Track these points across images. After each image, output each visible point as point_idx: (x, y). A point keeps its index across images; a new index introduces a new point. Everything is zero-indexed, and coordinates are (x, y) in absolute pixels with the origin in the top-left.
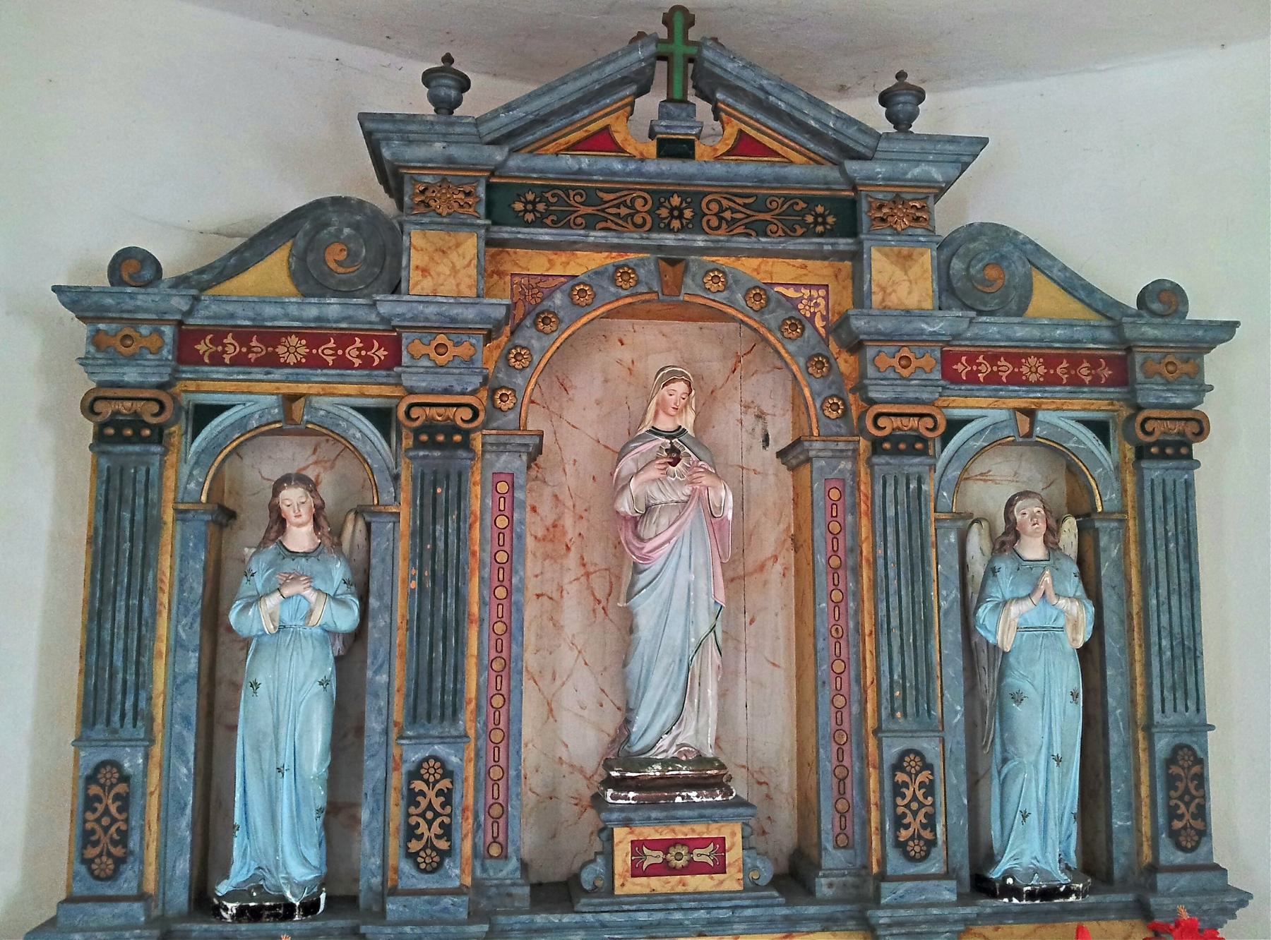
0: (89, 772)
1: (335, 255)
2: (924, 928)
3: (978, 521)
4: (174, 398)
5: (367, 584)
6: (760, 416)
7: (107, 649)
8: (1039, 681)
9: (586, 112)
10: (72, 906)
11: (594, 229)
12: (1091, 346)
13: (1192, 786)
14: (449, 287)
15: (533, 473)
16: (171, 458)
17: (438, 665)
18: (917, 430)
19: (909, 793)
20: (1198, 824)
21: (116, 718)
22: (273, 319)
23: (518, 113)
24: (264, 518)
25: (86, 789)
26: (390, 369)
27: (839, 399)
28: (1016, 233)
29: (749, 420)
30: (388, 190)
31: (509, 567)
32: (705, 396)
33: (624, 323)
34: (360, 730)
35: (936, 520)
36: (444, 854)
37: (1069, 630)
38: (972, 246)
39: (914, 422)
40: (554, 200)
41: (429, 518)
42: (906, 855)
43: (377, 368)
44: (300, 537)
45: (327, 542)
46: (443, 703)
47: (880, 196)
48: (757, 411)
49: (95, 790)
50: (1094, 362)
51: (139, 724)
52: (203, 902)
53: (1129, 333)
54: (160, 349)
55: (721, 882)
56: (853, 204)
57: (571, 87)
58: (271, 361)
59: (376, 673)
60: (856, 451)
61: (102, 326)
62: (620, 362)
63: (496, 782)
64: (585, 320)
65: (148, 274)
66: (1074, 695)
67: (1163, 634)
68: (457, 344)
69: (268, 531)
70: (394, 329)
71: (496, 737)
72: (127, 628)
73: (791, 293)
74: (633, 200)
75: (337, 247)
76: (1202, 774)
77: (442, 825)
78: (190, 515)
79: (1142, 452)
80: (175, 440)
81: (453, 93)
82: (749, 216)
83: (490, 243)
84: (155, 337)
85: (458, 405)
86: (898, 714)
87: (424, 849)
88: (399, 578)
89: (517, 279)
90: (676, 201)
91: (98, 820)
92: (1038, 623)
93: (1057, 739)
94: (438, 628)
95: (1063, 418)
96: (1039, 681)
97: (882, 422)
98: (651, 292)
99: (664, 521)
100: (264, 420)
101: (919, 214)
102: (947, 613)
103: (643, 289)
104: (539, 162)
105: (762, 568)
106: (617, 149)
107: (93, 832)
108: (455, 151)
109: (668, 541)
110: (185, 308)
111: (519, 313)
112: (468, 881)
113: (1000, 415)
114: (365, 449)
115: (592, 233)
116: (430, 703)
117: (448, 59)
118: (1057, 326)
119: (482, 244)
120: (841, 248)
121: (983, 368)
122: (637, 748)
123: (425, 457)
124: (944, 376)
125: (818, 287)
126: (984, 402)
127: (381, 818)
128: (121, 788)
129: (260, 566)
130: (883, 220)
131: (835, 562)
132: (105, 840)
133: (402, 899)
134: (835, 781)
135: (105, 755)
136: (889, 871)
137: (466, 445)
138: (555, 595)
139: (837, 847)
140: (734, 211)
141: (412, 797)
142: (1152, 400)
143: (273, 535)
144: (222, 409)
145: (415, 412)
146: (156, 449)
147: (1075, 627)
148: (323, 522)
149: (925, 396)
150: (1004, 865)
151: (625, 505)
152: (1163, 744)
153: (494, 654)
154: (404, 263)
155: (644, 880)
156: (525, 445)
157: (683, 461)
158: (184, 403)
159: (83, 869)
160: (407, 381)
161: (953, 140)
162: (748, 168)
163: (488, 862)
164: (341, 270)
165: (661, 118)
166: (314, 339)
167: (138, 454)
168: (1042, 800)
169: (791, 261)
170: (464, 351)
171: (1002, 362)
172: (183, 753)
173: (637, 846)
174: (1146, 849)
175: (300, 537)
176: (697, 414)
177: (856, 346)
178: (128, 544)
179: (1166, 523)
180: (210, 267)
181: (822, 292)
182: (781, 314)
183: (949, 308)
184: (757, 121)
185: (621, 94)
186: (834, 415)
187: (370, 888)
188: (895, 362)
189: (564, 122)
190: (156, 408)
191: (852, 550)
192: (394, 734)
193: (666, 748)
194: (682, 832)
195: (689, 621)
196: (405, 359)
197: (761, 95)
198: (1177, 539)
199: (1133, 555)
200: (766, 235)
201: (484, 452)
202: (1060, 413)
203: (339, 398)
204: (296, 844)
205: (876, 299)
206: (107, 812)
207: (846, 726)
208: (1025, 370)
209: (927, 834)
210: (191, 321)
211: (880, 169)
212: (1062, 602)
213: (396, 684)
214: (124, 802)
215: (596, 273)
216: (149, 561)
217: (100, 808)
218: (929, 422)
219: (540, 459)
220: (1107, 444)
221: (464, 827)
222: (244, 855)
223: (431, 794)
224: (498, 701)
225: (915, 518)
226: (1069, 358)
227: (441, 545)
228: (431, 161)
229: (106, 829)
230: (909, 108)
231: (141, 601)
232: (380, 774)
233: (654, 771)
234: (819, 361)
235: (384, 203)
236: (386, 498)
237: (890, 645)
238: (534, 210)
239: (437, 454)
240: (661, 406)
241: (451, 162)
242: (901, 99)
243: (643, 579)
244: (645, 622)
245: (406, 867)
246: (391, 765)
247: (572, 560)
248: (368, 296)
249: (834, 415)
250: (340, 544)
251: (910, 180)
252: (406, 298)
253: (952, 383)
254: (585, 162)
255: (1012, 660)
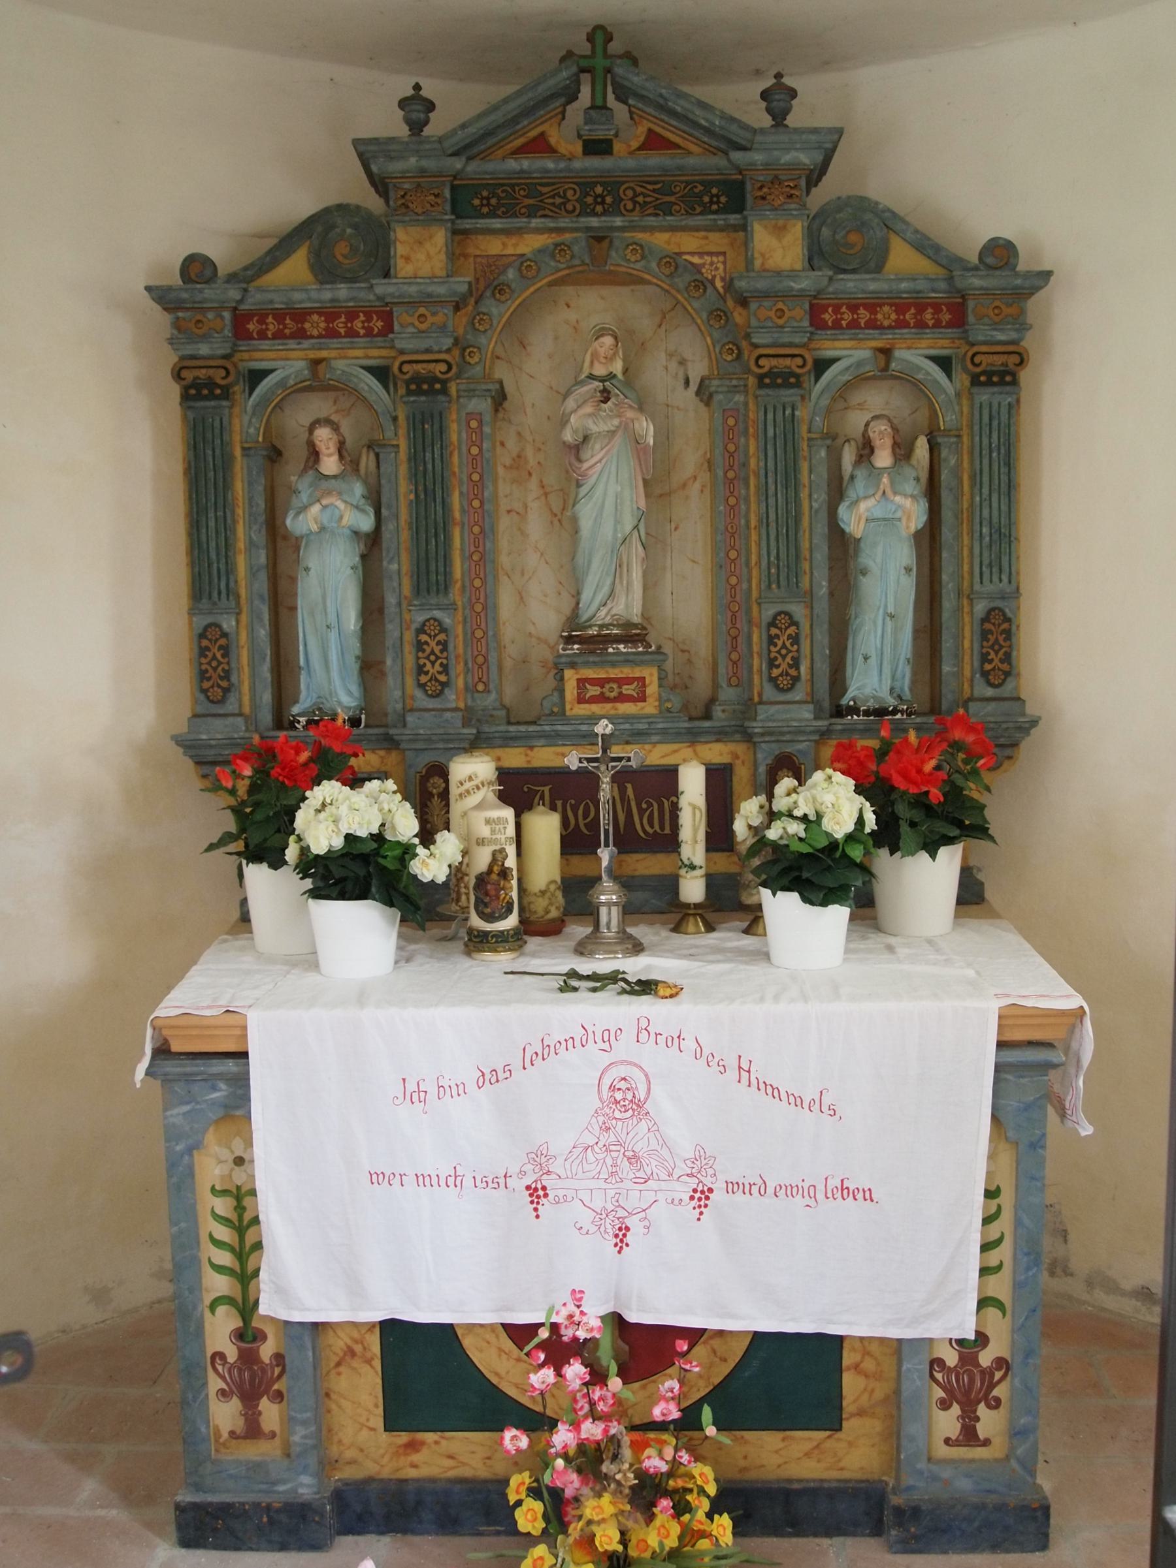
0: (200, 631)
1: (341, 249)
2: (788, 737)
3: (848, 441)
4: (235, 365)
5: (379, 493)
6: (682, 362)
7: (205, 546)
8: (879, 560)
9: (525, 123)
10: (198, 720)
11: (535, 217)
12: (934, 295)
13: (1001, 639)
14: (425, 270)
15: (500, 415)
16: (236, 410)
17: (432, 554)
18: (789, 367)
19: (780, 643)
20: (1005, 667)
21: (215, 594)
22: (300, 302)
23: (472, 130)
24: (304, 453)
25: (200, 642)
26: (385, 335)
27: (734, 344)
28: (877, 203)
29: (673, 365)
30: (377, 191)
31: (479, 485)
32: (632, 345)
33: (570, 289)
34: (381, 610)
35: (809, 439)
36: (444, 685)
37: (904, 521)
38: (838, 216)
39: (788, 361)
40: (503, 195)
41: (420, 448)
42: (777, 686)
43: (377, 335)
44: (330, 464)
45: (349, 468)
46: (437, 581)
47: (761, 178)
48: (680, 356)
49: (205, 643)
50: (937, 307)
51: (231, 598)
52: (282, 721)
53: (959, 284)
54: (222, 329)
55: (643, 708)
56: (742, 183)
57: (511, 106)
58: (301, 335)
59: (389, 563)
60: (746, 386)
61: (180, 314)
62: (567, 322)
63: (479, 640)
64: (532, 289)
65: (208, 272)
66: (908, 570)
67: (984, 523)
68: (434, 314)
69: (307, 462)
70: (387, 304)
71: (478, 608)
72: (217, 532)
73: (696, 260)
74: (565, 192)
75: (343, 244)
76: (1010, 630)
77: (441, 665)
78: (252, 452)
79: (975, 381)
80: (237, 397)
81: (422, 116)
82: (657, 199)
83: (455, 232)
84: (219, 320)
85: (437, 361)
86: (774, 586)
87: (430, 680)
88: (401, 493)
89: (479, 260)
90: (599, 190)
91: (209, 663)
92: (884, 515)
93: (891, 600)
94: (431, 529)
95: (914, 355)
96: (879, 560)
97: (762, 362)
98: (583, 264)
99: (598, 447)
100: (298, 380)
101: (793, 192)
102: (817, 511)
103: (576, 262)
104: (490, 166)
105: (684, 486)
106: (551, 150)
107: (207, 671)
108: (424, 163)
109: (600, 461)
110: (238, 297)
111: (482, 286)
112: (462, 705)
113: (865, 354)
114: (372, 398)
115: (534, 220)
116: (428, 580)
117: (417, 87)
118: (902, 280)
119: (449, 235)
120: (732, 222)
121: (846, 316)
122: (584, 618)
123: (414, 402)
124: (811, 325)
125: (718, 254)
126: (849, 344)
127: (399, 664)
128: (223, 641)
129: (304, 487)
130: (763, 198)
131: (731, 474)
132: (215, 676)
133: (417, 714)
134: (729, 639)
135: (210, 619)
136: (765, 698)
137: (444, 391)
138: (521, 510)
139: (730, 685)
140: (645, 196)
141: (420, 646)
142: (981, 338)
143: (310, 464)
144: (272, 371)
145: (406, 368)
146: (225, 403)
147: (909, 519)
148: (345, 454)
149: (797, 340)
150: (850, 693)
151: (568, 436)
152: (980, 608)
153: (473, 549)
154: (392, 253)
155: (586, 706)
156: (489, 390)
157: (613, 400)
158: (241, 368)
159: (202, 697)
160: (399, 344)
161: (815, 131)
162: (655, 160)
163: (476, 695)
164: (347, 261)
165: (586, 124)
166: (330, 316)
167: (214, 407)
168: (879, 646)
169: (696, 234)
170: (439, 319)
171: (862, 311)
172: (261, 620)
173: (581, 683)
174: (966, 686)
175: (330, 464)
176: (624, 361)
177: (744, 302)
178: (212, 473)
179: (990, 437)
180: (252, 265)
181: (721, 258)
182: (688, 278)
183: (820, 269)
184: (662, 120)
185: (552, 107)
186: (729, 358)
187: (395, 711)
188: (772, 314)
189: (509, 132)
190: (223, 373)
191: (744, 465)
192: (404, 606)
193: (603, 616)
194: (614, 673)
195: (617, 521)
196: (396, 327)
197: (661, 101)
198: (999, 449)
199: (966, 464)
200: (672, 214)
201: (459, 397)
202: (913, 351)
203: (350, 361)
204: (343, 679)
205: (758, 263)
206: (214, 658)
207: (738, 598)
208: (879, 316)
209: (793, 672)
210: (242, 307)
211: (758, 157)
212: (898, 499)
213: (404, 569)
214: (226, 651)
215: (540, 251)
216: (227, 486)
217: (210, 655)
218: (799, 361)
219: (506, 404)
220: (949, 376)
221: (457, 669)
222: (308, 688)
223: (433, 644)
224: (477, 583)
225: (790, 436)
226: (916, 305)
227: (430, 466)
228: (408, 172)
229: (215, 669)
230: (782, 104)
231: (225, 513)
232: (397, 634)
233: (593, 631)
234: (719, 315)
235: (373, 202)
236: (389, 434)
237: (768, 534)
238: (488, 205)
239: (423, 398)
240: (595, 356)
241: (422, 172)
242: (777, 97)
243: (583, 491)
244: (586, 524)
245: (419, 694)
246: (404, 626)
247: (533, 484)
248: (367, 281)
249: (729, 358)
250: (358, 470)
251: (784, 164)
252: (394, 281)
253: (817, 329)
254: (525, 164)
255: (862, 545)
